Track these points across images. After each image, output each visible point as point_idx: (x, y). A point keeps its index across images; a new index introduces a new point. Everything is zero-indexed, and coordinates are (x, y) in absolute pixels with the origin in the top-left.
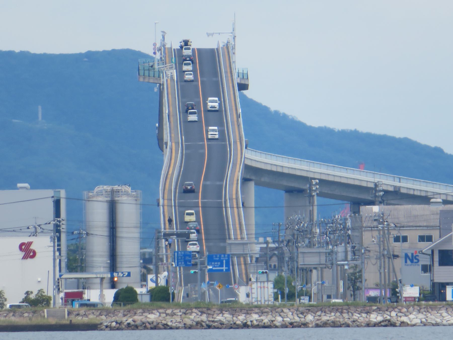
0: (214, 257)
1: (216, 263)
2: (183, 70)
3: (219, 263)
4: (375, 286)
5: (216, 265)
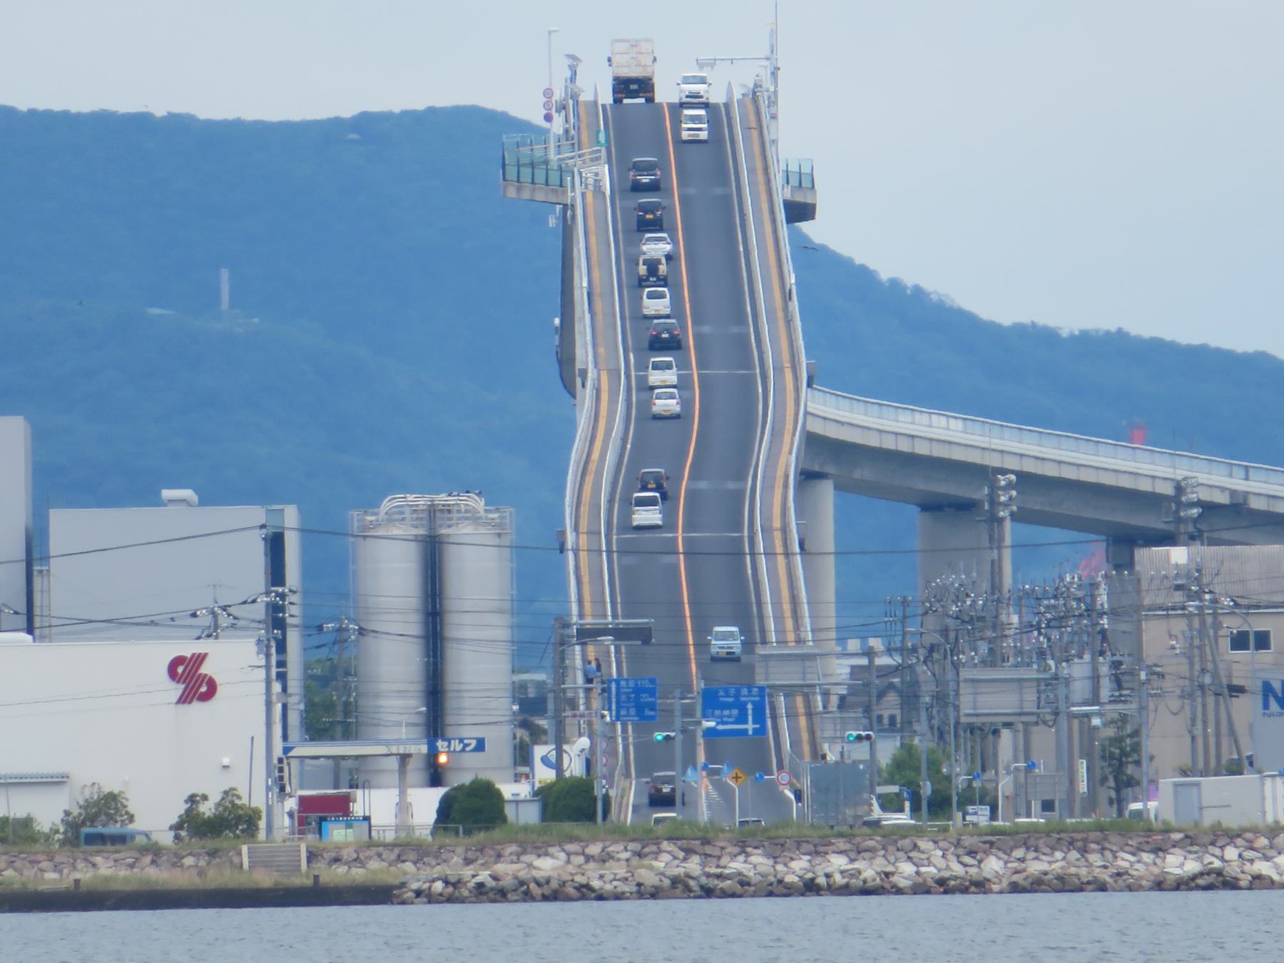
1: (726, 712)
3: (735, 712)
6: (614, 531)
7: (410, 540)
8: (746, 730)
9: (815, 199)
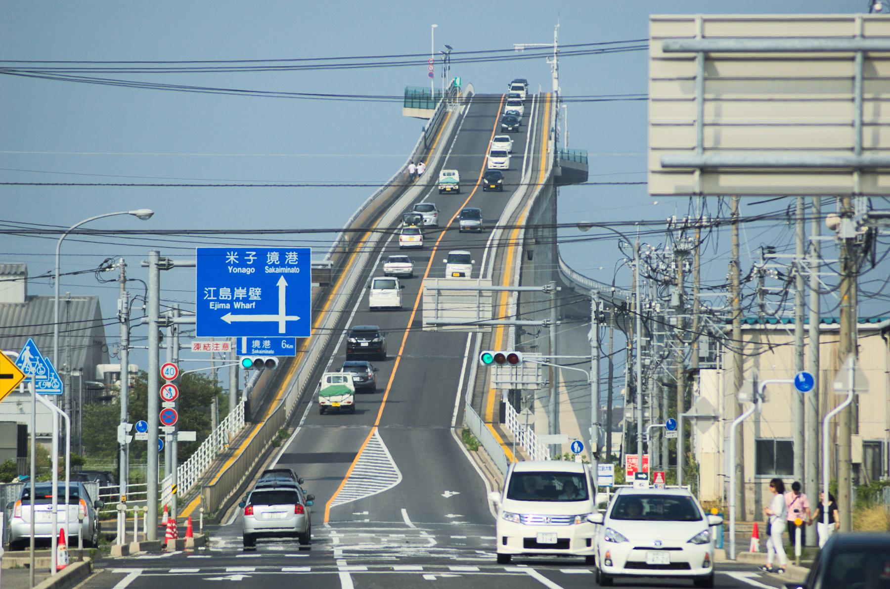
0: (232, 258)
1: (240, 293)
2: (371, 305)
3: (255, 293)
4: (659, 168)
5: (238, 300)
6: (450, 151)
7: (804, 227)
8: (276, 324)
9: (588, 169)
